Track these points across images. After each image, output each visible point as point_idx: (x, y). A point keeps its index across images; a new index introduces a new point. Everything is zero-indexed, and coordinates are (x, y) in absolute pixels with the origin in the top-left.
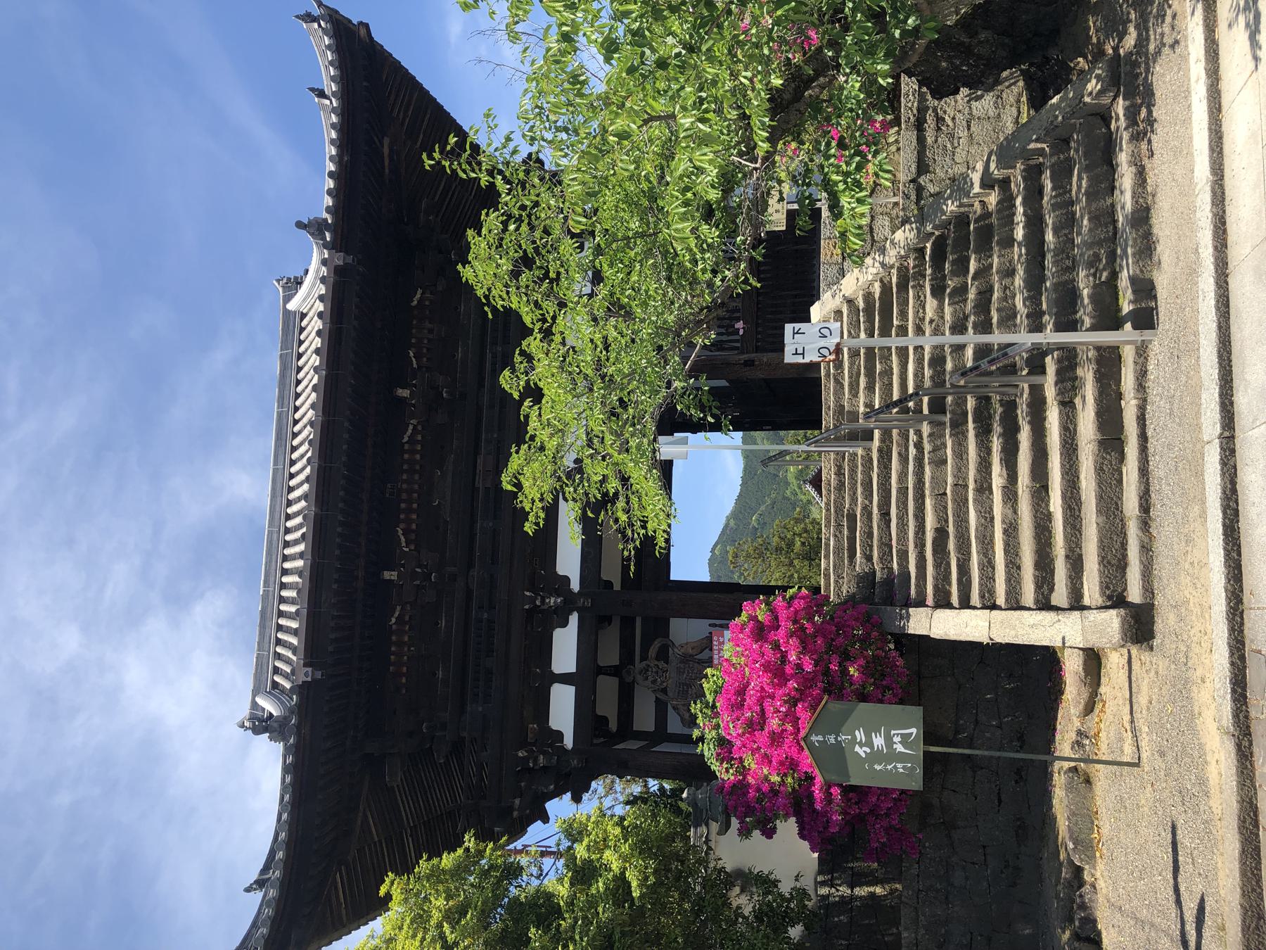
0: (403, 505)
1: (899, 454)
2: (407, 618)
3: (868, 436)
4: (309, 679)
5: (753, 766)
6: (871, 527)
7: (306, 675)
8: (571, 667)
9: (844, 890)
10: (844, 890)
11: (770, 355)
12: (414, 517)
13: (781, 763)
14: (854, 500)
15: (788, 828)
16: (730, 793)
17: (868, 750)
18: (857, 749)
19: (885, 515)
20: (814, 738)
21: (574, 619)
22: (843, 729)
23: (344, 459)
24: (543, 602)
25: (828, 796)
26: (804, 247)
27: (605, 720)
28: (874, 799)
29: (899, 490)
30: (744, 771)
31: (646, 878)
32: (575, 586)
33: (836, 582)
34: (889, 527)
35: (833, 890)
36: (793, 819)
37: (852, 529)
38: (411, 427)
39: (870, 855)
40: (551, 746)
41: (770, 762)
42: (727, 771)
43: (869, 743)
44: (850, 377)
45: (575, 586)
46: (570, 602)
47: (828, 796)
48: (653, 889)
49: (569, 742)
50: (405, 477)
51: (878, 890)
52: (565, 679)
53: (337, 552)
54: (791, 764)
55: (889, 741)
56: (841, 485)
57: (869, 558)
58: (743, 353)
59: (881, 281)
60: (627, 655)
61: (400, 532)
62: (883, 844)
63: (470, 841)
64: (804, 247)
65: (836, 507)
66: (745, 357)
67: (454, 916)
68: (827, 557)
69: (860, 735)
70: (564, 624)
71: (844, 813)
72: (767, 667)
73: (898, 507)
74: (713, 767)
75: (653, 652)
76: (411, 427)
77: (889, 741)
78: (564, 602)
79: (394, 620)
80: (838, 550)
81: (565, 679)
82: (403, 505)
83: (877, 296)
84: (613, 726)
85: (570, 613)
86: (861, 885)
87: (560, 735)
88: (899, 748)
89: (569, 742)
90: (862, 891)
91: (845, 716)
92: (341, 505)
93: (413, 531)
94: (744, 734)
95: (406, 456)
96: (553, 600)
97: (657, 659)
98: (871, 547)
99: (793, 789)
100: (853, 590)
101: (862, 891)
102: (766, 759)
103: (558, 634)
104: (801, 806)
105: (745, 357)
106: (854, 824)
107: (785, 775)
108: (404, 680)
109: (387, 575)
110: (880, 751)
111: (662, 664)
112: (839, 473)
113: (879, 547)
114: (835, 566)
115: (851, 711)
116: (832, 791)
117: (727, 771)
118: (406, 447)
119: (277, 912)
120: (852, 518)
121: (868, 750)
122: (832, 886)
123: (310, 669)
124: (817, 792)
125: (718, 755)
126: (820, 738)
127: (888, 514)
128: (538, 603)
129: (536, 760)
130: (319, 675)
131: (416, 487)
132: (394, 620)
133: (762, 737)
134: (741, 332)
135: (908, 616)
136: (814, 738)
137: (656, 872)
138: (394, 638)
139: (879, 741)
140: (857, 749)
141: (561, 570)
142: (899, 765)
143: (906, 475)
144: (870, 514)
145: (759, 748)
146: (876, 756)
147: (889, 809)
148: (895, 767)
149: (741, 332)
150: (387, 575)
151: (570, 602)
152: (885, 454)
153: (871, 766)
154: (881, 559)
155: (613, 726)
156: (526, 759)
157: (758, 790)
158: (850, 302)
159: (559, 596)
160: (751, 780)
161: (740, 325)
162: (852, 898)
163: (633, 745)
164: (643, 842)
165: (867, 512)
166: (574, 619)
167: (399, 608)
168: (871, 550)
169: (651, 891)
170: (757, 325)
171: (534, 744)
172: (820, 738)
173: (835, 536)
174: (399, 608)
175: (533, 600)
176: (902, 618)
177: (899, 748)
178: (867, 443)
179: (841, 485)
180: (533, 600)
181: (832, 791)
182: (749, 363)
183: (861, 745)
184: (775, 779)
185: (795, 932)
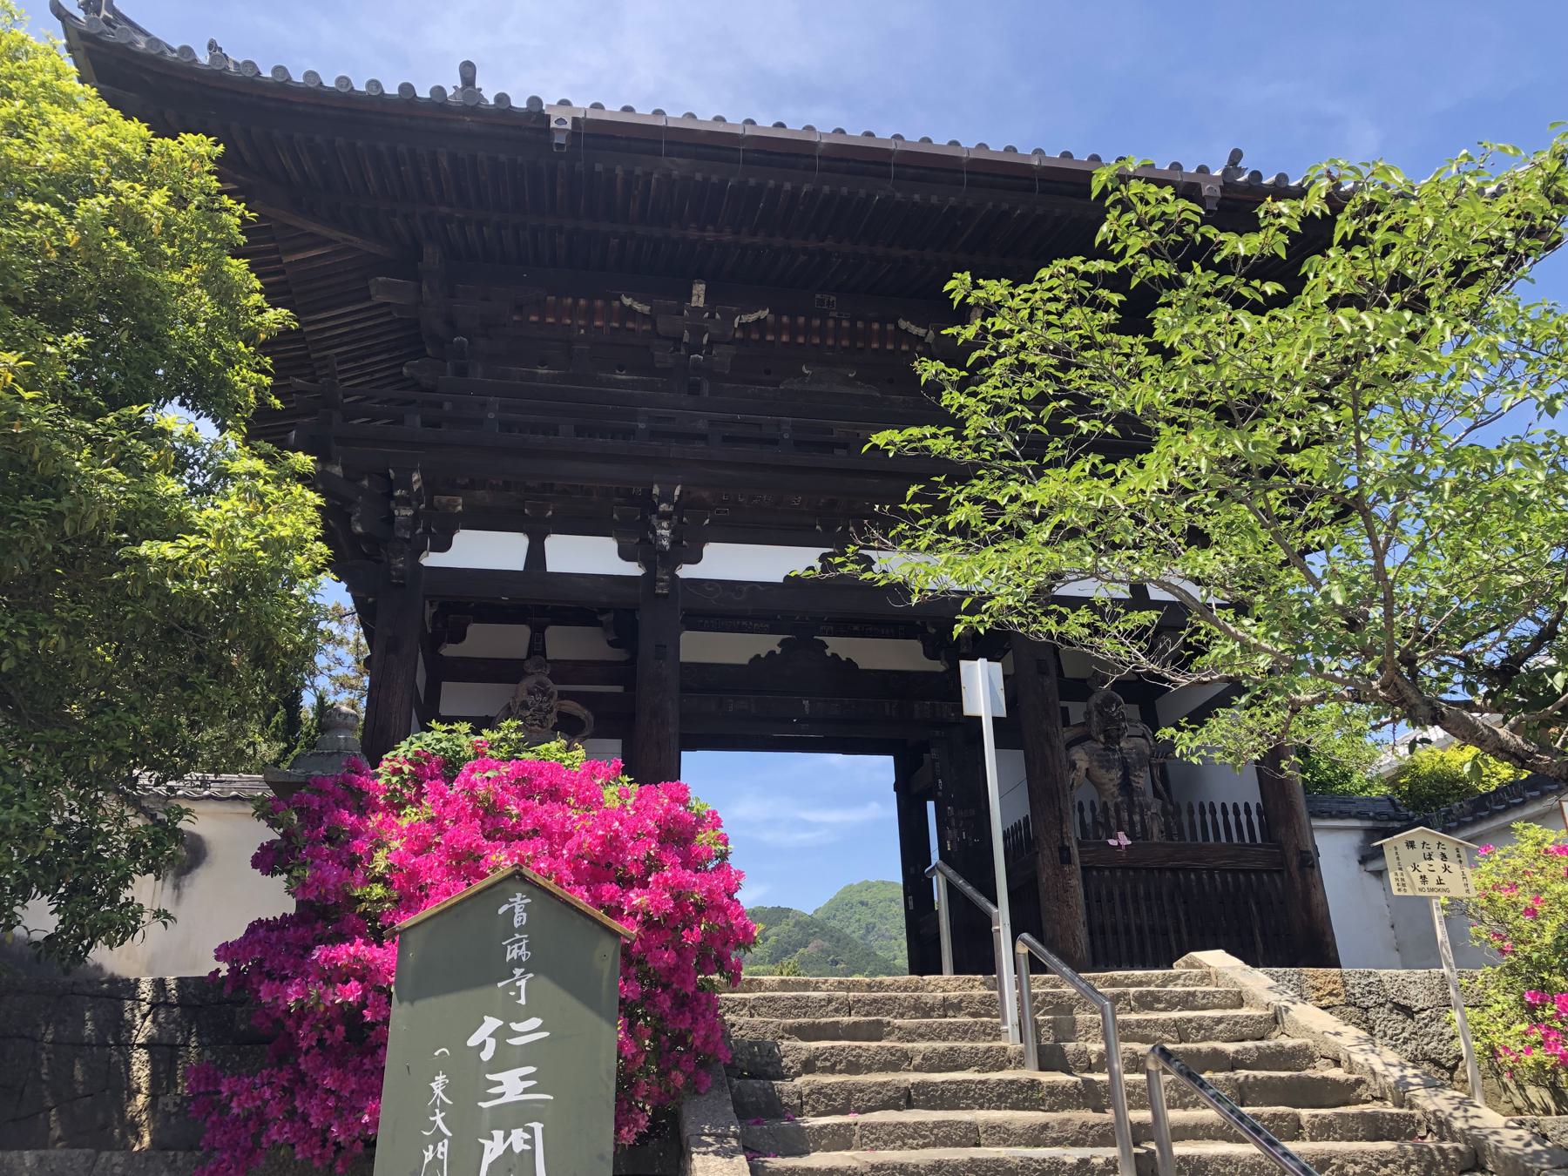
0: (801, 320)
1: (1045, 1127)
2: (630, 325)
3: (1050, 1059)
4: (553, 125)
5: (404, 823)
6: (869, 1070)
7: (561, 121)
8: (553, 566)
9: (144, 1030)
10: (144, 1030)
11: (1081, 891)
12: (785, 338)
13: (414, 875)
14: (910, 1035)
15: (273, 899)
16: (348, 783)
17: (486, 1055)
18: (491, 1023)
19: (908, 1098)
20: (519, 901)
21: (633, 569)
22: (544, 981)
23: (898, 195)
24: (665, 516)
25: (340, 976)
26: (1260, 946)
27: (459, 637)
28: (328, 1082)
29: (972, 1128)
30: (395, 806)
31: (178, 577)
32: (686, 572)
33: (743, 1003)
34: (886, 1106)
35: (145, 1008)
36: (291, 909)
37: (853, 1032)
38: (922, 332)
39: (206, 1078)
40: (427, 531)
41: (417, 854)
42: (396, 772)
43: (503, 1061)
44: (1139, 1024)
45: (686, 572)
46: (659, 560)
47: (340, 976)
48: (154, 589)
49: (432, 560)
50: (845, 324)
51: (141, 1100)
52: (536, 555)
53: (752, 182)
54: (411, 897)
55: (513, 1116)
56: (924, 1010)
57: (809, 1066)
58: (1080, 844)
59: (1359, 1082)
60: (564, 671)
61: (763, 314)
62: (228, 1106)
63: (275, 317)
64: (1260, 946)
65: (884, 1001)
66: (1075, 851)
67: (130, 222)
68: (784, 986)
69: (529, 1030)
70: (625, 554)
71: (302, 1014)
72: (612, 844)
73: (937, 1125)
74: (404, 745)
75: (571, 707)
76: (922, 332)
77: (513, 1116)
78: (662, 551)
79: (627, 301)
80: (801, 1006)
81: (536, 555)
82: (801, 320)
83: (1309, 1072)
84: (449, 650)
85: (644, 562)
86: (153, 1061)
87: (444, 545)
88: (493, 1149)
89: (432, 560)
90: (140, 1068)
91: (578, 985)
92: (826, 189)
93: (763, 337)
94: (474, 798)
95: (876, 326)
96: (666, 533)
97: (560, 714)
98: (832, 1070)
99: (359, 900)
100: (736, 1034)
101: (140, 1068)
102: (419, 844)
103: (609, 545)
104: (325, 914)
105: (1075, 851)
106: (274, 1040)
107: (387, 884)
108: (533, 318)
109: (699, 289)
110: (484, 1090)
111: (552, 719)
112: (947, 1007)
113: (842, 1086)
114: (772, 999)
115: (589, 998)
116: (354, 984)
117: (396, 772)
118: (890, 327)
119: (170, 65)
120: (875, 1031)
121: (486, 1055)
122: (153, 1005)
123: (569, 126)
124: (359, 949)
125: (428, 758)
126: (520, 918)
127: (910, 1104)
128: (663, 507)
129: (405, 502)
130: (560, 139)
131: (830, 342)
132: (627, 301)
133: (470, 834)
134: (1112, 842)
135: (730, 1154)
136: (519, 901)
137: (195, 599)
138: (599, 303)
139: (512, 1085)
140: (491, 1023)
141: (710, 549)
142: (443, 1148)
143: (1004, 1142)
144: (894, 1066)
145: (442, 830)
146: (471, 1079)
147: (305, 1119)
148: (439, 1136)
149: (1112, 842)
150: (699, 289)
151: (659, 560)
152: (1024, 1097)
153: (442, 1065)
154: (819, 1091)
155: (449, 650)
156: (408, 485)
157: (355, 833)
158: (1276, 1020)
159: (672, 543)
160: (374, 821)
161: (1124, 840)
162: (126, 1046)
163: (421, 679)
164: (259, 583)
165: (897, 1062)
166: (633, 569)
167: (646, 309)
168: (824, 1070)
169: (151, 583)
170: (1125, 869)
171: (430, 505)
172: (520, 918)
173: (830, 1001)
174: (646, 309)
175: (666, 497)
176: (720, 1138)
177: (493, 1149)
178: (1032, 1059)
179: (924, 1010)
180: (666, 497)
181: (354, 984)
182: (1065, 856)
183: (501, 1034)
184: (381, 862)
185: (39, 917)
